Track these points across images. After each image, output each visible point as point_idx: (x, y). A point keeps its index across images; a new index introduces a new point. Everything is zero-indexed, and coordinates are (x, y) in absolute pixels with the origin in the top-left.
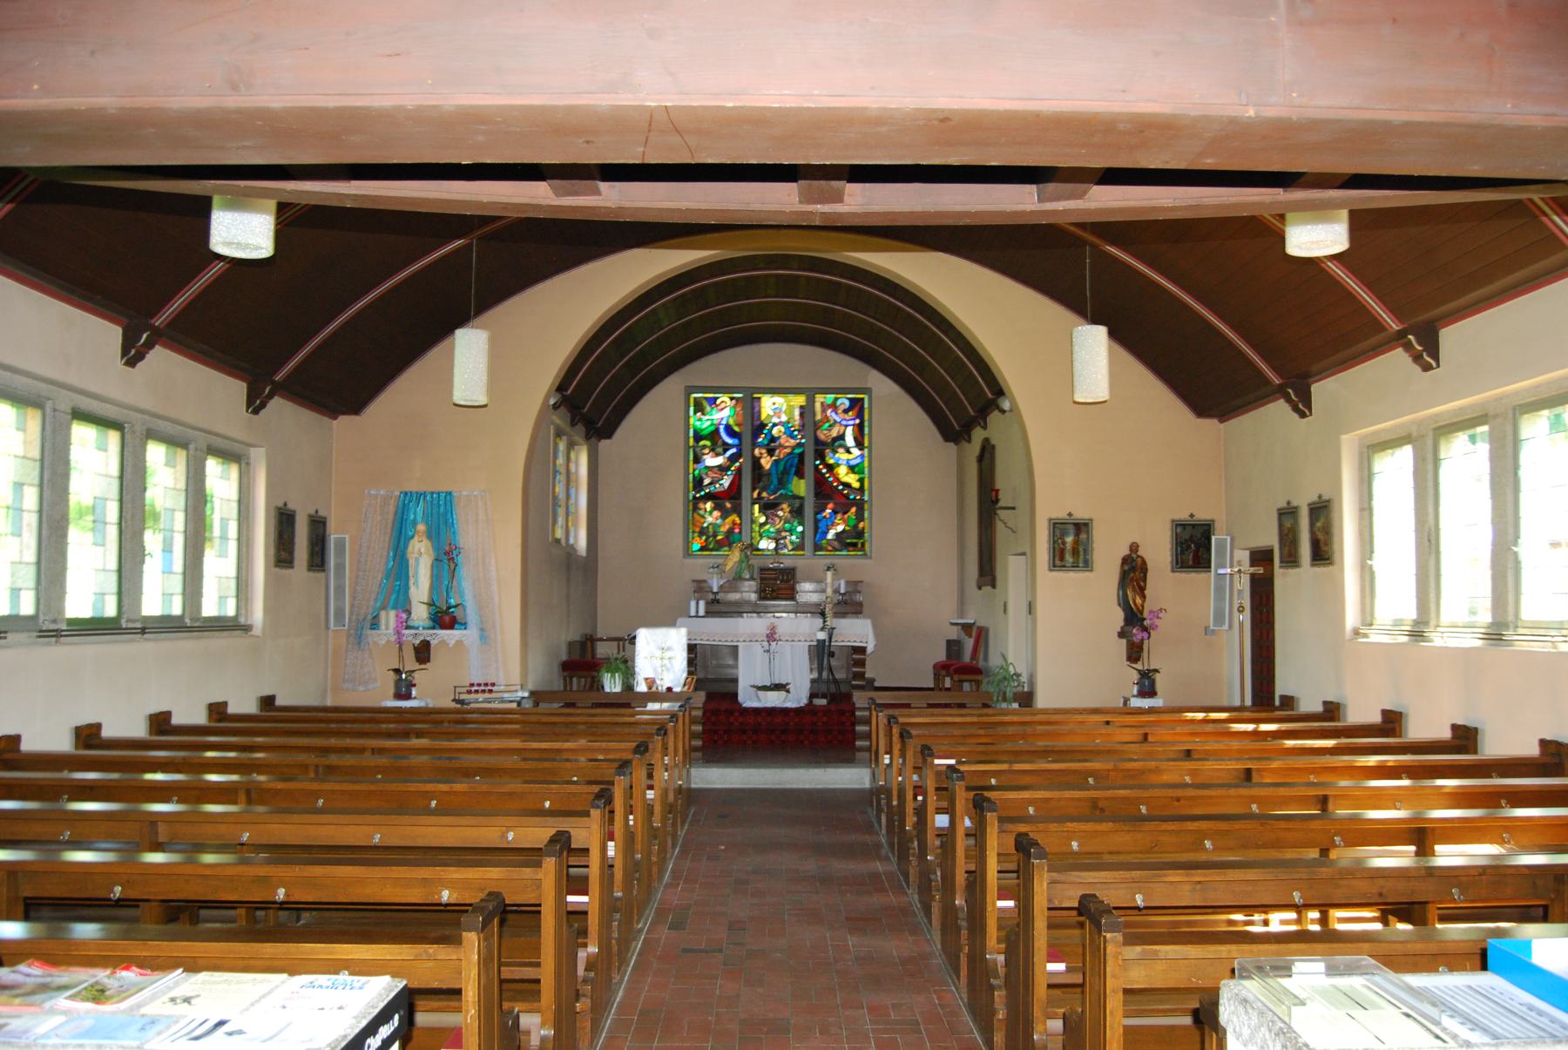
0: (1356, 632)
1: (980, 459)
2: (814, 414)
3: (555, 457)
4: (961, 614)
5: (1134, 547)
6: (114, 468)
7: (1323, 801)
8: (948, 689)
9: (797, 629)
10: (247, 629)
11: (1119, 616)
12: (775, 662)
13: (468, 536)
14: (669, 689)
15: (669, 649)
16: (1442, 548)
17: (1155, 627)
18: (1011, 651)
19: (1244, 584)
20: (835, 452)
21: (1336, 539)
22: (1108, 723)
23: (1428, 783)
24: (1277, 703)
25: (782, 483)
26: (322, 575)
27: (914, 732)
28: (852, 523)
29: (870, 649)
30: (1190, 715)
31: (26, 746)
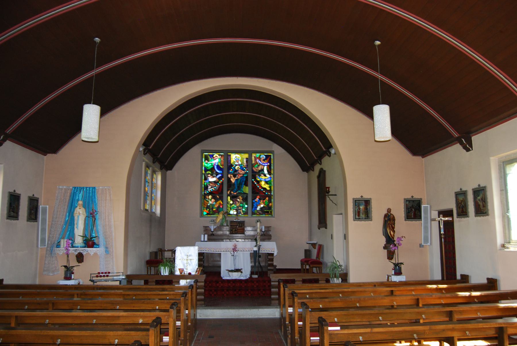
0: (503, 246)
1: (319, 177)
2: (252, 161)
5: (389, 210)
9: (245, 246)
11: (383, 241)
12: (236, 260)
14: (190, 274)
15: (190, 256)
17: (400, 244)
18: (335, 254)
20: (260, 176)
25: (239, 188)
28: (267, 203)
29: (275, 254)
30: (430, 286)
31: (5, 283)
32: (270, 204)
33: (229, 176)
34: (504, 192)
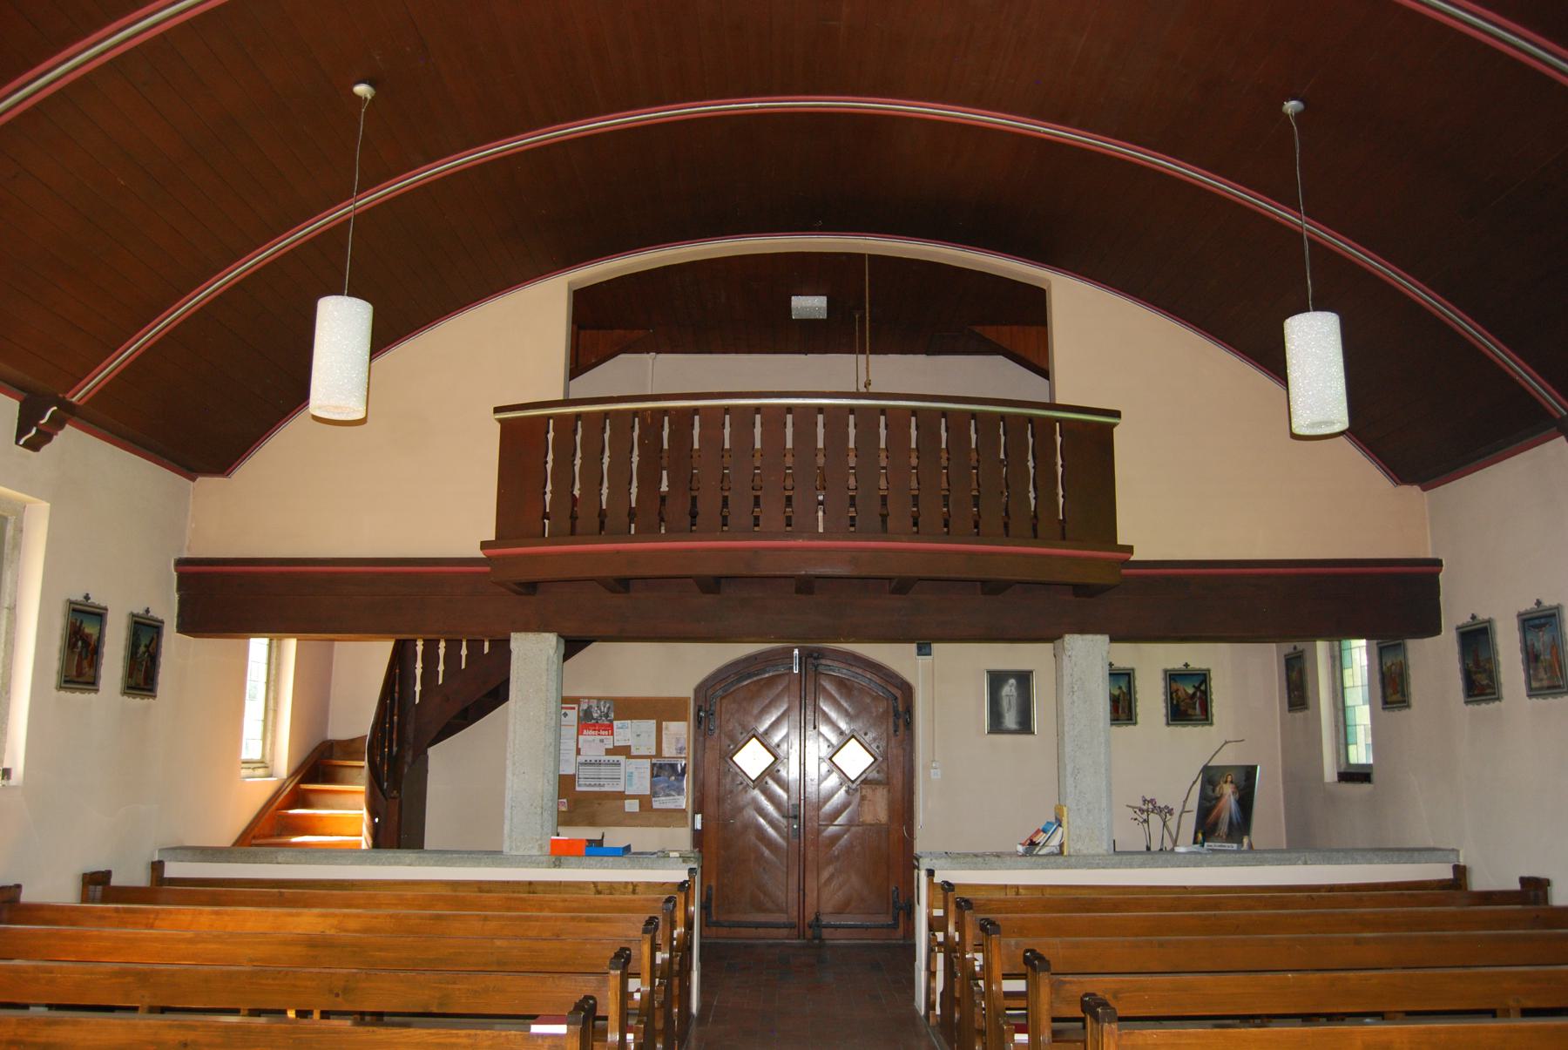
31: (26, 897)
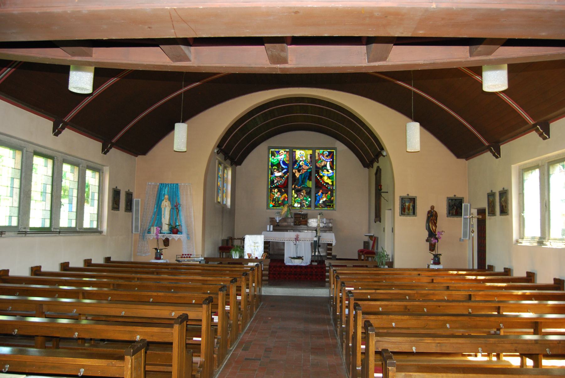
0: (517, 241)
1: (376, 174)
2: (315, 157)
3: (218, 172)
4: (369, 232)
5: (432, 207)
6: (50, 173)
7: (498, 309)
8: (363, 260)
9: (307, 236)
10: (101, 232)
11: (426, 234)
12: (298, 249)
13: (183, 200)
14: (256, 258)
15: (257, 243)
16: (551, 209)
19: (475, 222)
20: (323, 171)
21: (509, 205)
22: (419, 274)
23: (545, 302)
24: (487, 268)
25: (303, 182)
26: (131, 213)
27: (340, 277)
28: (329, 197)
29: (334, 244)
30: (451, 272)
31: (11, 274)
32: (332, 198)
33: (294, 171)
34: (521, 195)
